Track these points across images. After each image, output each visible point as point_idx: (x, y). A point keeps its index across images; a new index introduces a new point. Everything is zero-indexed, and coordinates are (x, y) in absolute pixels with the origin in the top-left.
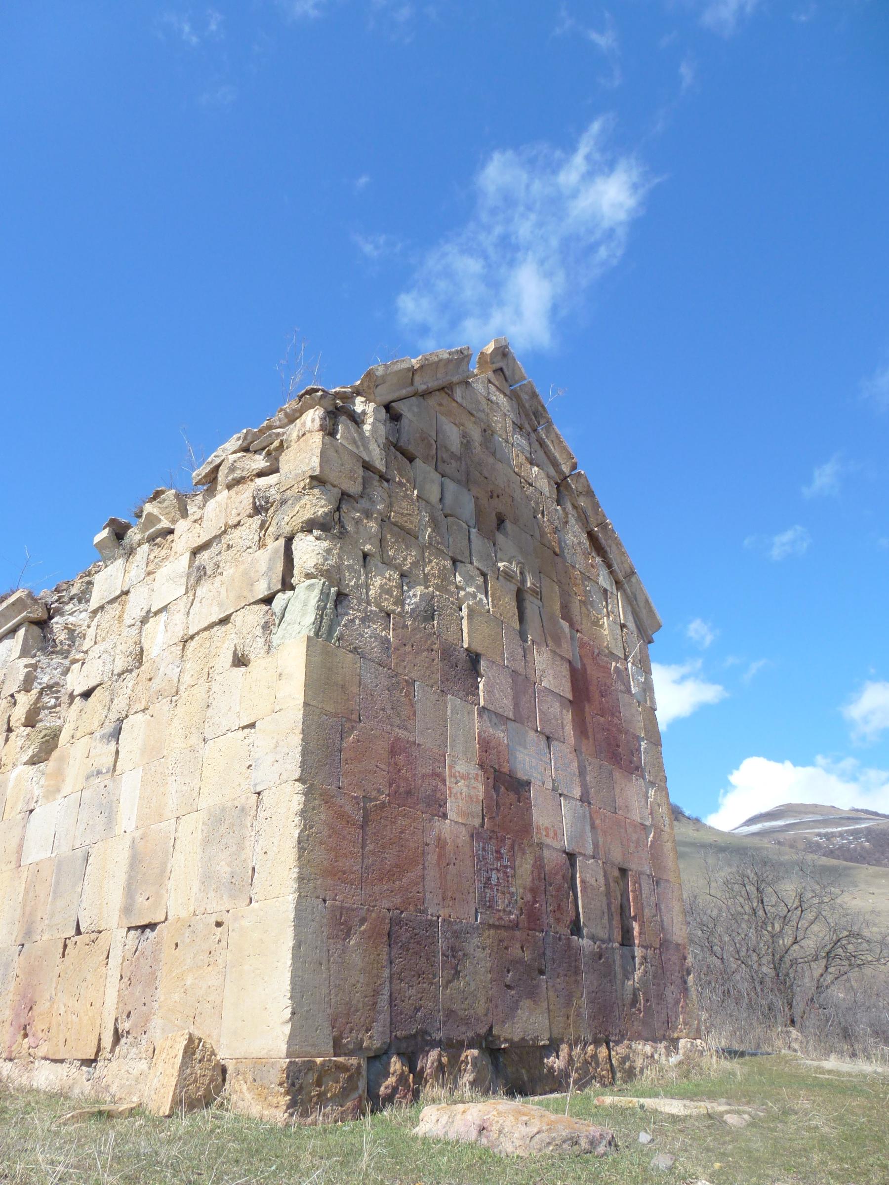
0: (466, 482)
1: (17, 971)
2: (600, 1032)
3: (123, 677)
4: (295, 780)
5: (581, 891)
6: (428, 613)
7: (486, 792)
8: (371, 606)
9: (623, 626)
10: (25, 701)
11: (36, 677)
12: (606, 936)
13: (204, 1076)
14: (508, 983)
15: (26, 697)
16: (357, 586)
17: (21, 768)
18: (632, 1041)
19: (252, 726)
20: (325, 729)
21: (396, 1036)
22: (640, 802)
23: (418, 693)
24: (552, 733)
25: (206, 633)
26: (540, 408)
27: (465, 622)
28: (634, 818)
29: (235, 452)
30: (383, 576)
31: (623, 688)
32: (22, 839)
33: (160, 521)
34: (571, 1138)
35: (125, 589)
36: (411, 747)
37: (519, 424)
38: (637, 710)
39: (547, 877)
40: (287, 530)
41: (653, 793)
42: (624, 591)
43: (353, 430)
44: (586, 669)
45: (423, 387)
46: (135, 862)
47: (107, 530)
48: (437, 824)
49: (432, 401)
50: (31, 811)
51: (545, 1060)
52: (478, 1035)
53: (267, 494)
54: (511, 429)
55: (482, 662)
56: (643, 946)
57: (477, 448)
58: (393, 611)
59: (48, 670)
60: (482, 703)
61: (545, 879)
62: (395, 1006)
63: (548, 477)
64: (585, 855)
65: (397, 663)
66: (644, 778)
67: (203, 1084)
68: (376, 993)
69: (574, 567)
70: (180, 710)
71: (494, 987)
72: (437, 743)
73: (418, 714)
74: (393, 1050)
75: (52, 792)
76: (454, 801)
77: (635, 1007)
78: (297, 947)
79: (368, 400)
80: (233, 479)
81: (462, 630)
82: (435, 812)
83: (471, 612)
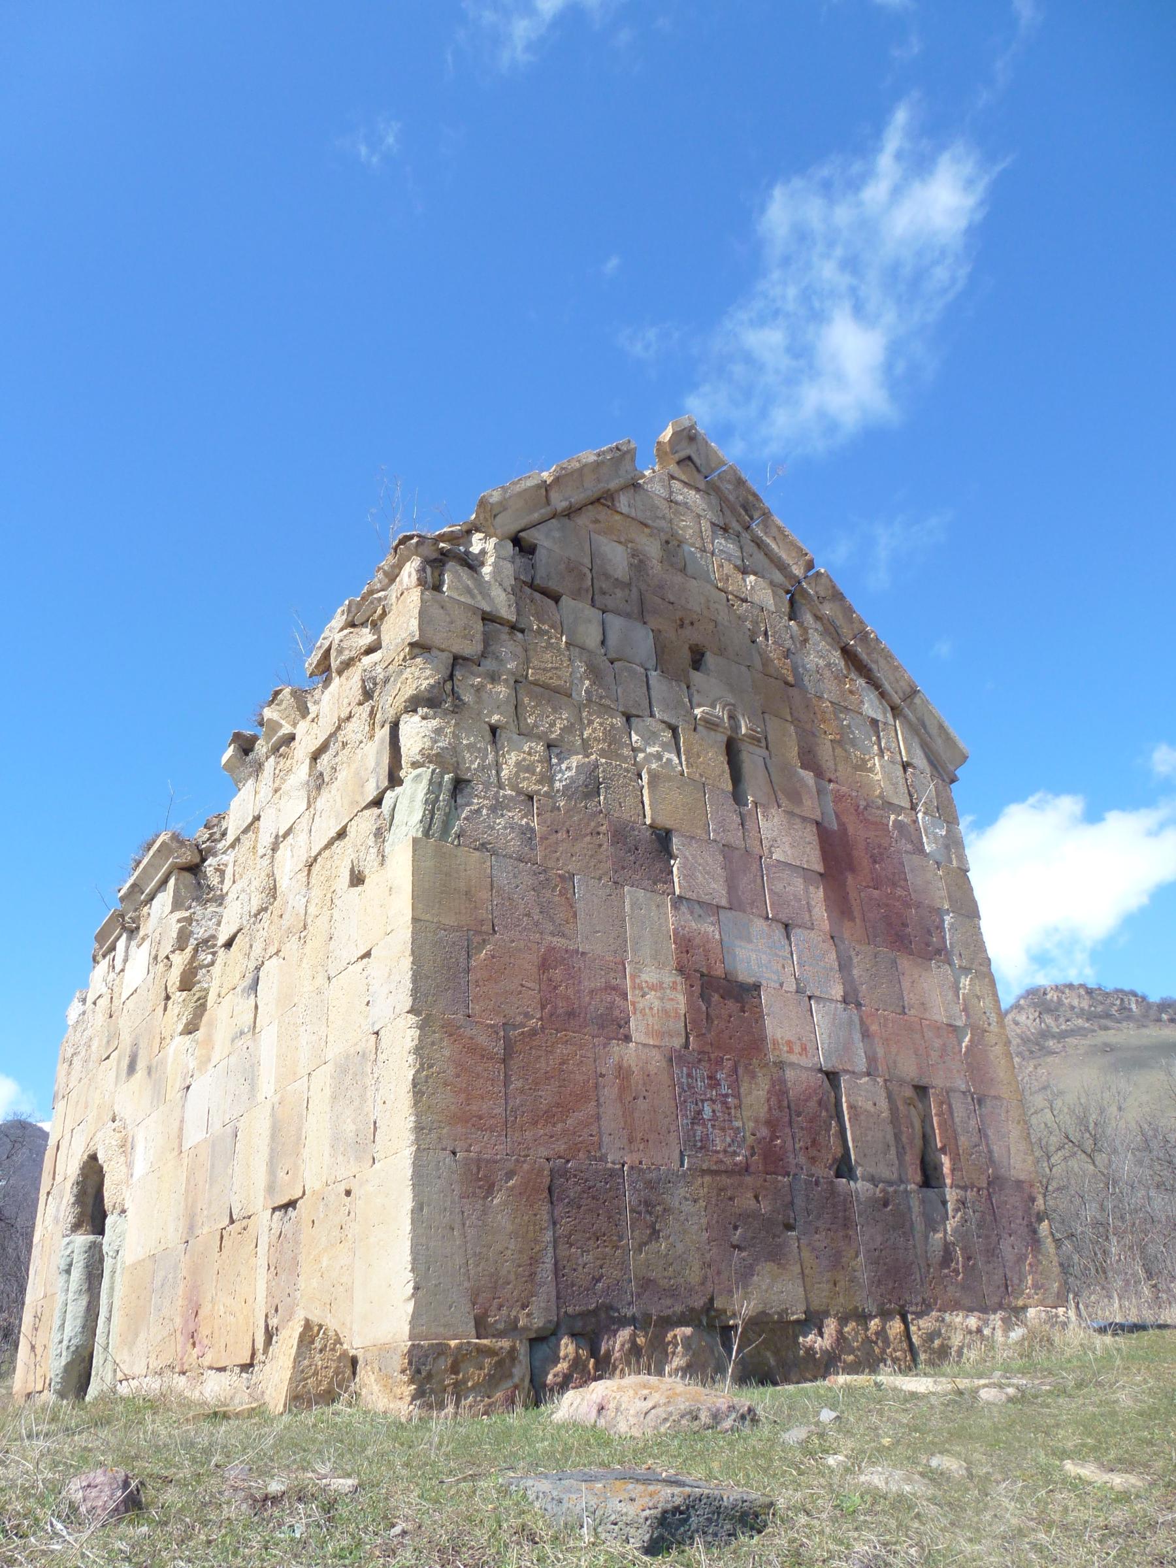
0: (641, 613)
1: (184, 1273)
2: (890, 1301)
3: (259, 917)
4: (408, 1012)
5: (850, 1119)
6: (590, 786)
7: (690, 1003)
8: (504, 789)
9: (905, 766)
10: (180, 960)
11: (192, 932)
12: (895, 1177)
13: (327, 1367)
14: (735, 1243)
15: (181, 957)
16: (482, 768)
17: (179, 1039)
18: (945, 1312)
19: (367, 955)
20: (445, 947)
21: (566, 1312)
22: (946, 995)
23: (580, 889)
24: (791, 918)
25: (327, 853)
26: (751, 498)
27: (645, 792)
28: (936, 1017)
29: (342, 630)
30: (520, 750)
31: (909, 847)
33: (281, 726)
34: (691, 1412)
35: (256, 814)
36: (572, 956)
37: (722, 524)
38: (936, 874)
39: (792, 1105)
40: (391, 713)
41: (967, 983)
42: (905, 717)
43: (465, 577)
44: (846, 829)
45: (565, 504)
47: (232, 746)
48: (616, 1049)
49: (583, 520)
50: (188, 1088)
51: (801, 1339)
52: (692, 1310)
53: (373, 674)
54: (709, 533)
55: (674, 840)
56: (958, 1187)
57: (656, 567)
58: (537, 792)
59: (203, 922)
60: (677, 892)
61: (789, 1107)
62: (563, 1276)
63: (772, 584)
64: (854, 1073)
65: (546, 856)
66: (950, 963)
67: (325, 1377)
68: (534, 1261)
69: (820, 698)
71: (714, 1250)
72: (612, 948)
73: (581, 915)
74: (563, 1329)
76: (640, 1018)
77: (949, 1267)
78: (418, 1210)
79: (488, 536)
80: (341, 663)
81: (643, 803)
82: (611, 1035)
83: (654, 778)
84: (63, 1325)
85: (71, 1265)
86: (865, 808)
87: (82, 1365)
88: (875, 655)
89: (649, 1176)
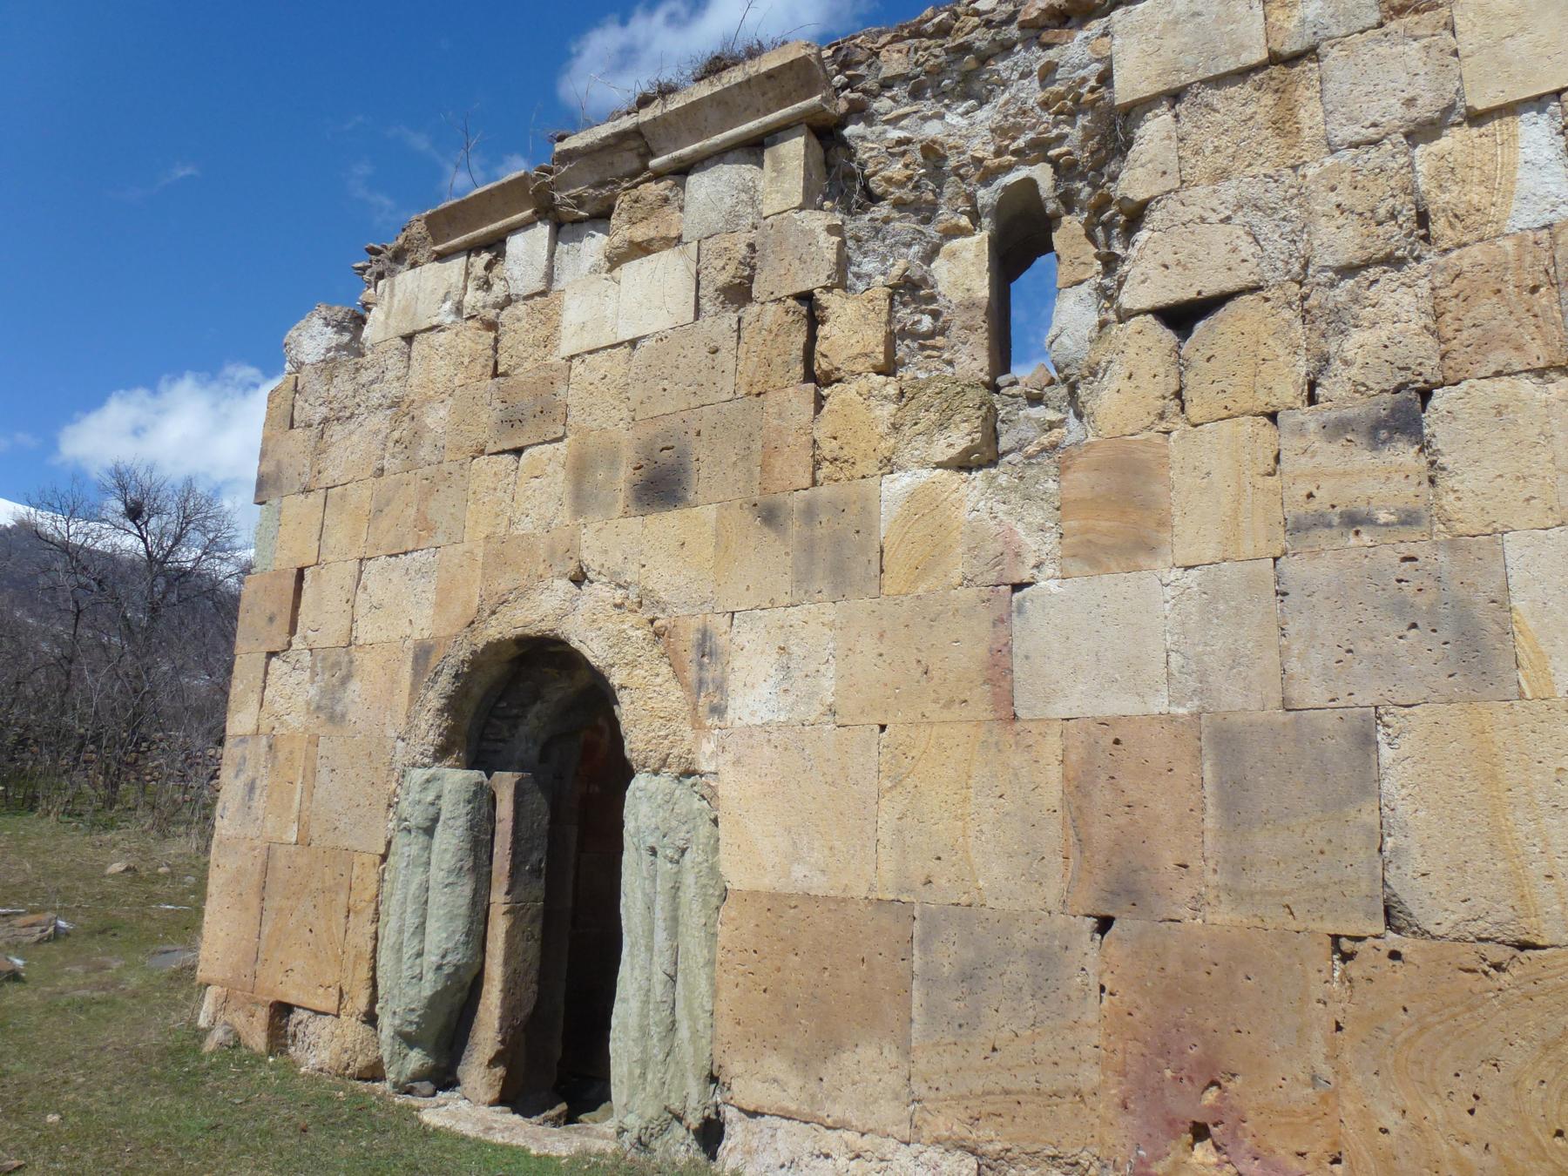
84: (421, 928)
85: (435, 820)
87: (459, 995)
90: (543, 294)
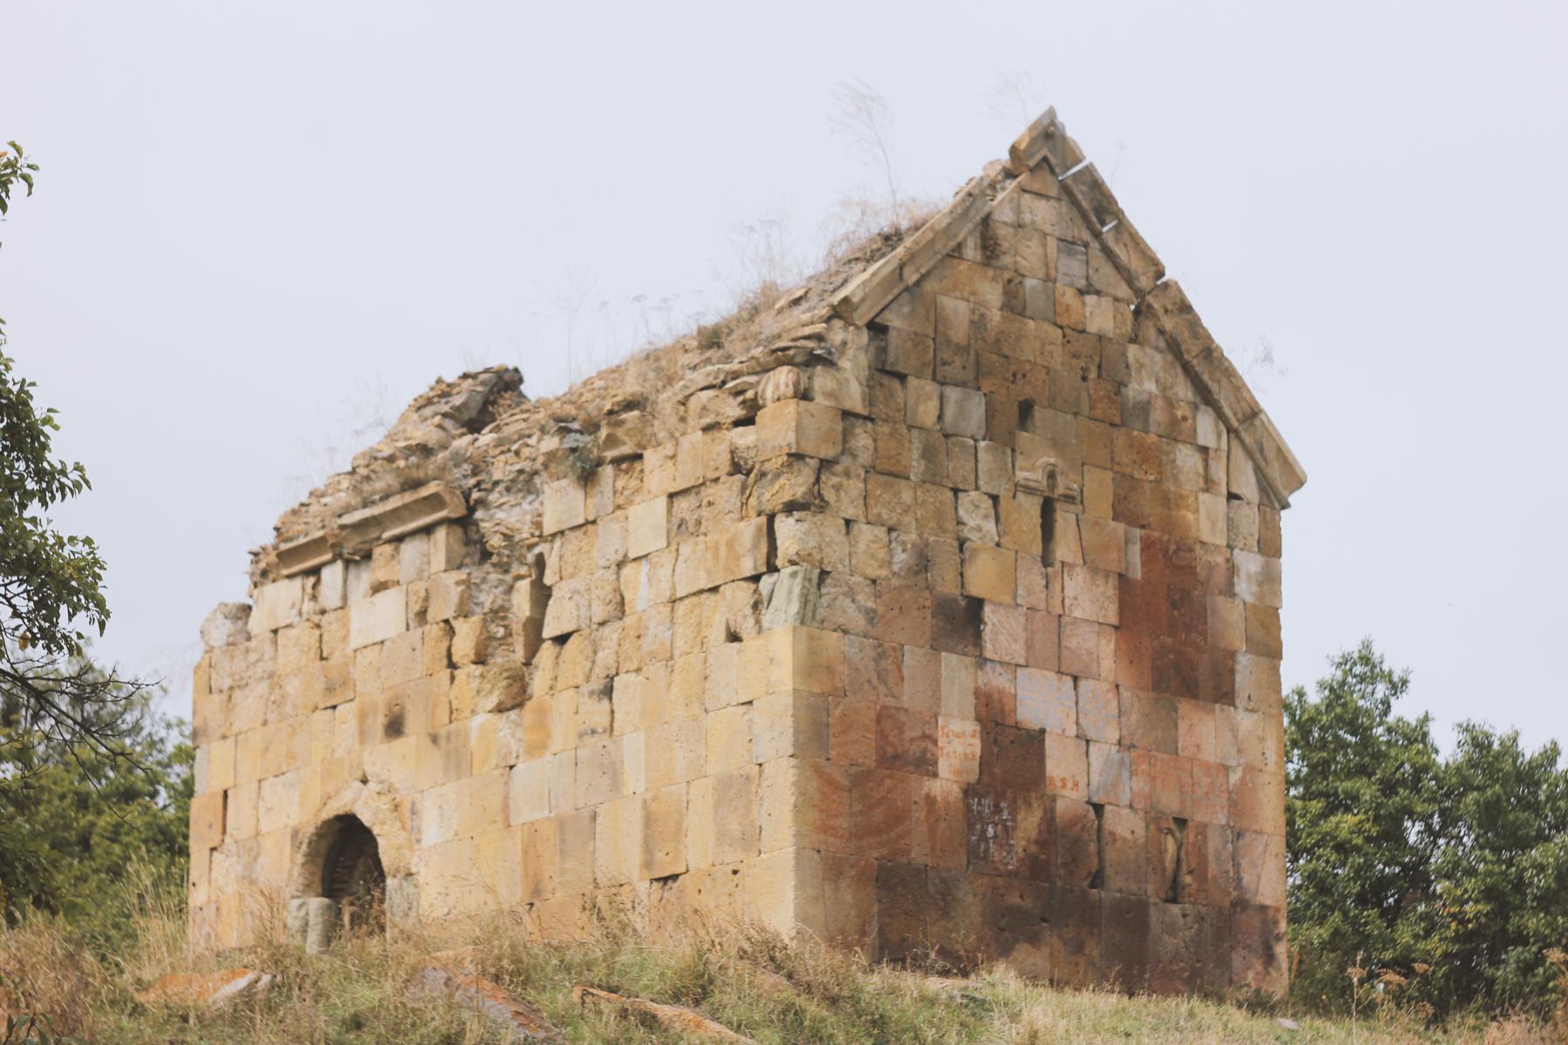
19: (750, 703)
25: (695, 599)
32: (506, 797)
46: (649, 822)
50: (511, 767)
57: (995, 316)
59: (484, 586)
70: (677, 677)
75: (537, 748)
86: (1175, 552)
88: (1218, 374)
89: (944, 874)
90: (342, 608)
